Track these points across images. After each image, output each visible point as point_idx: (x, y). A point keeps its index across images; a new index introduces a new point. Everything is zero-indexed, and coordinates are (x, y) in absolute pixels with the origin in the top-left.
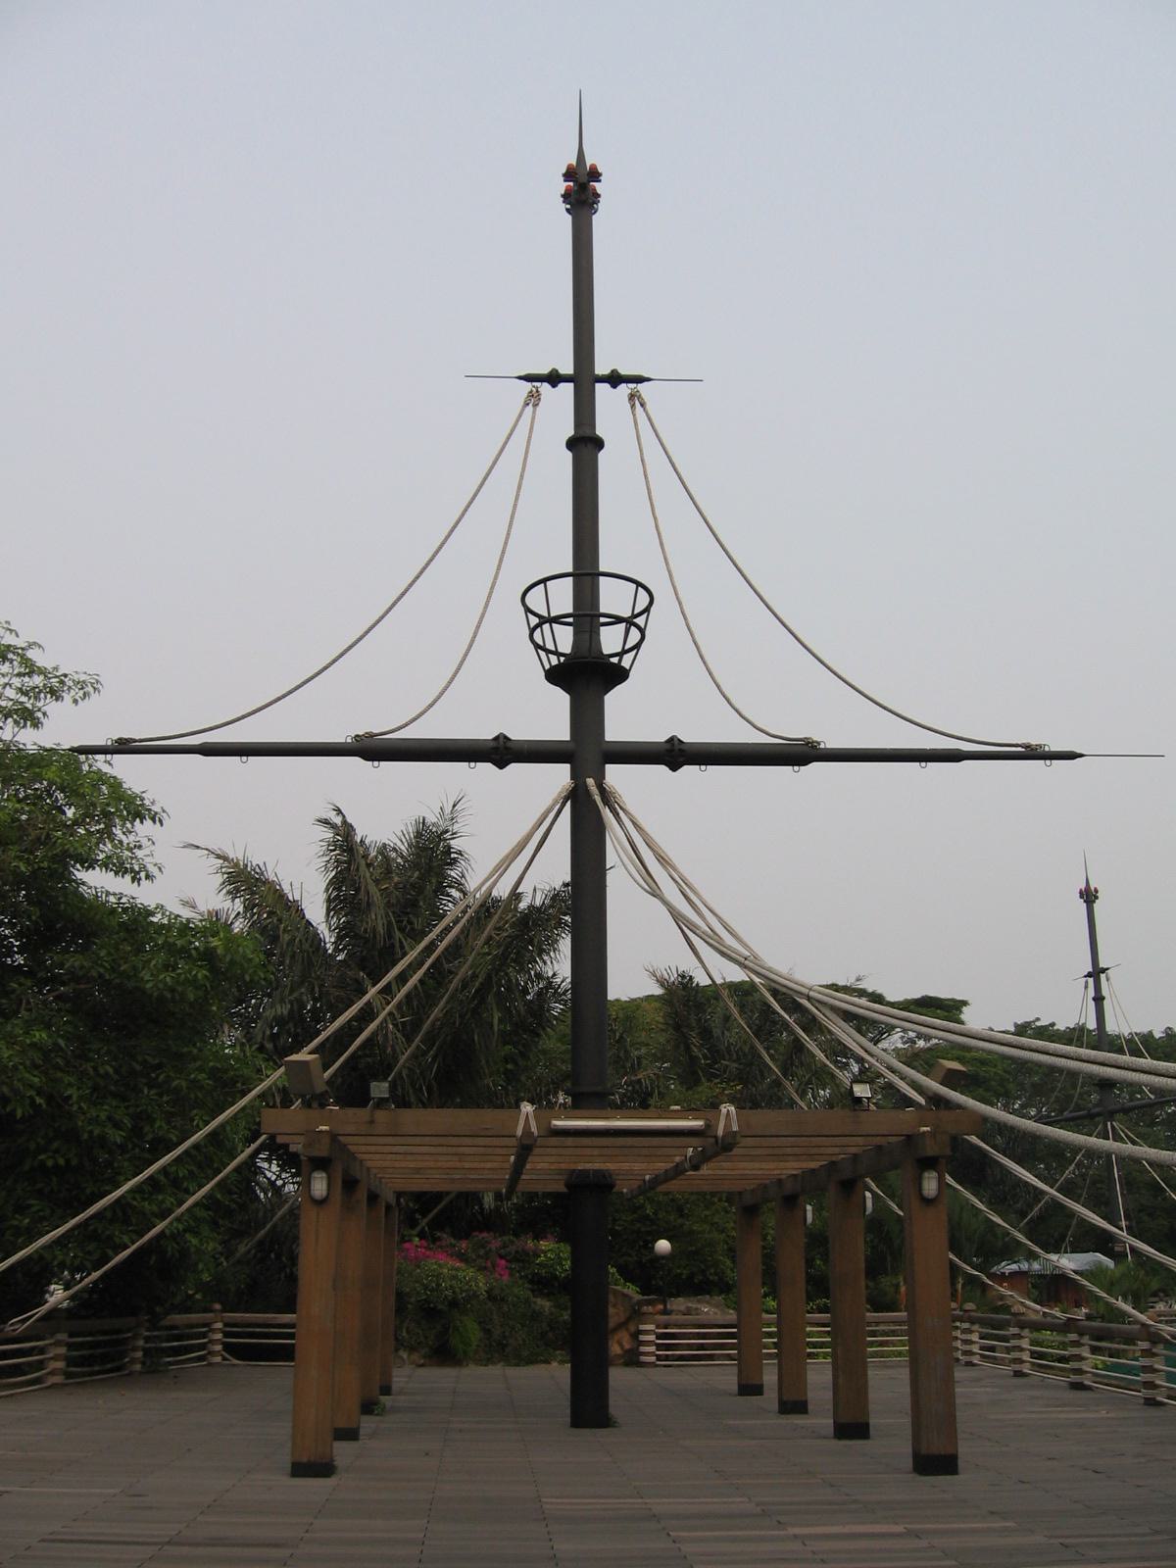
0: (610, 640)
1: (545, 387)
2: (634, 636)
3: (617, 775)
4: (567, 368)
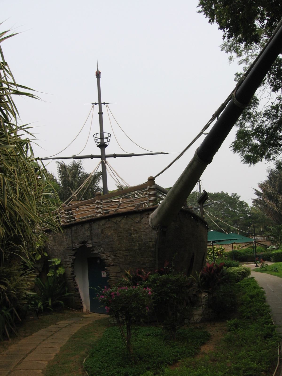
1: (95, 105)
3: (107, 159)
4: (98, 102)
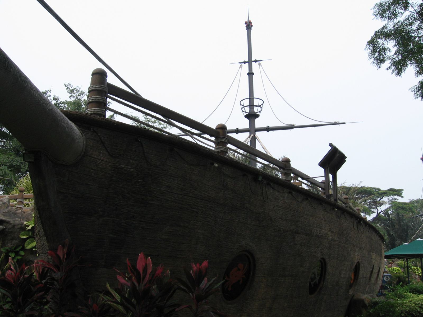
0: (256, 110)
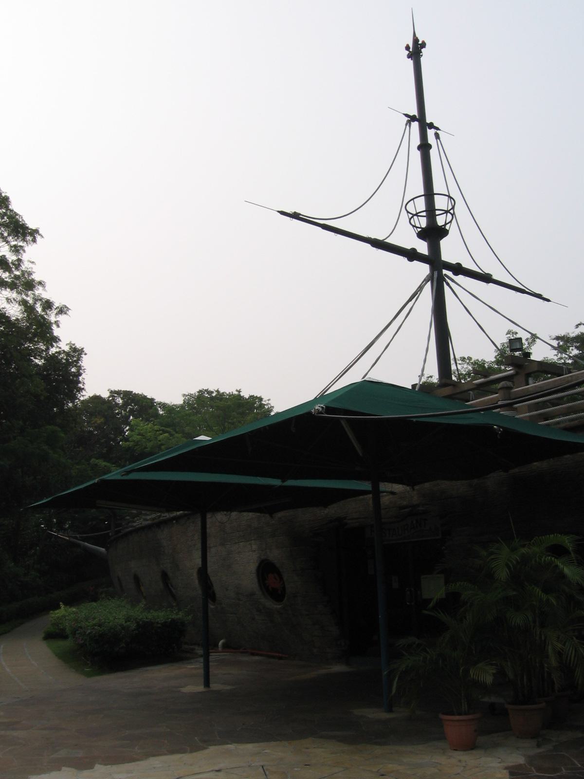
0: (440, 221)
2: (449, 216)
